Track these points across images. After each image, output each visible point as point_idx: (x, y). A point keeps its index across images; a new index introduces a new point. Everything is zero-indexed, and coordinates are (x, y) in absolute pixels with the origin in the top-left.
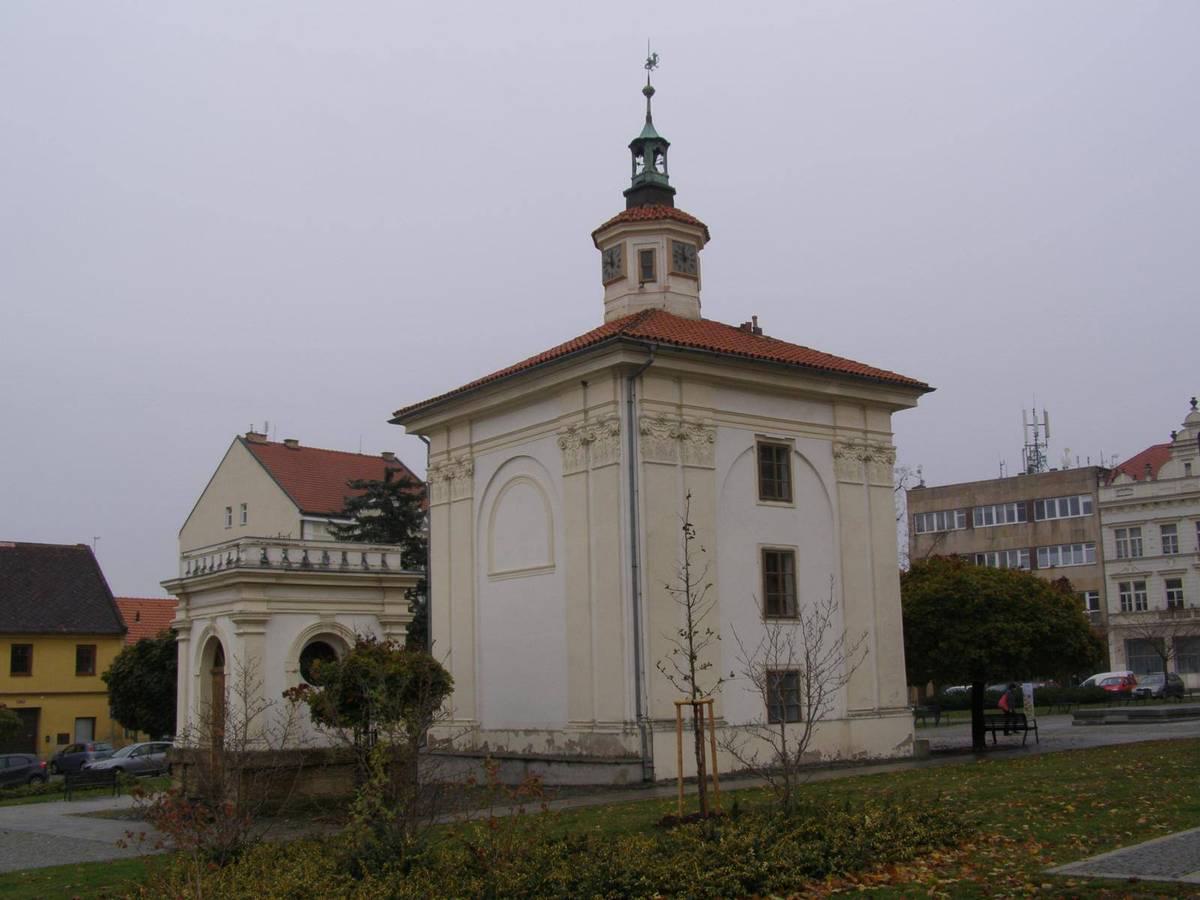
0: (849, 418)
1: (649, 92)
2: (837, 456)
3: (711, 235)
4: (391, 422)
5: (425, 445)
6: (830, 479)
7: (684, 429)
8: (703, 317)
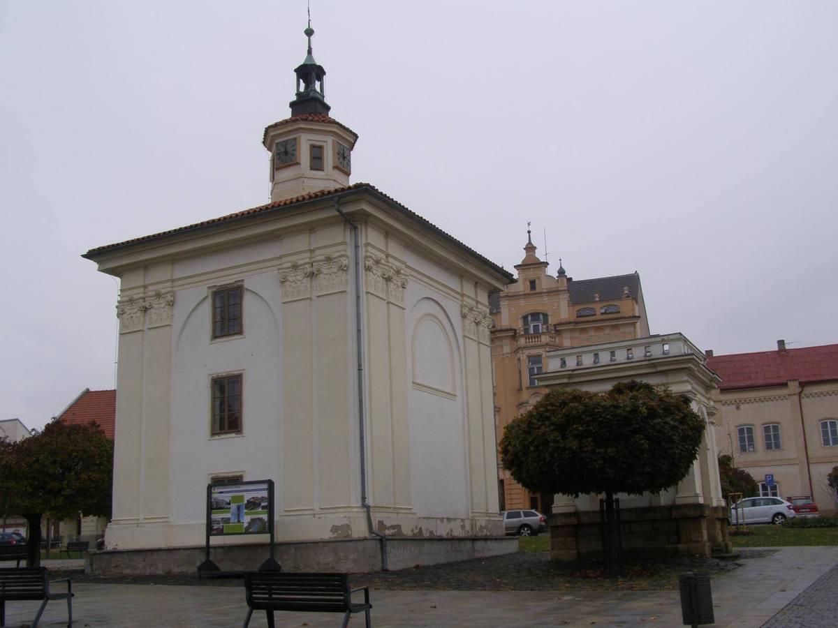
1: (309, 33)
7: (314, 270)
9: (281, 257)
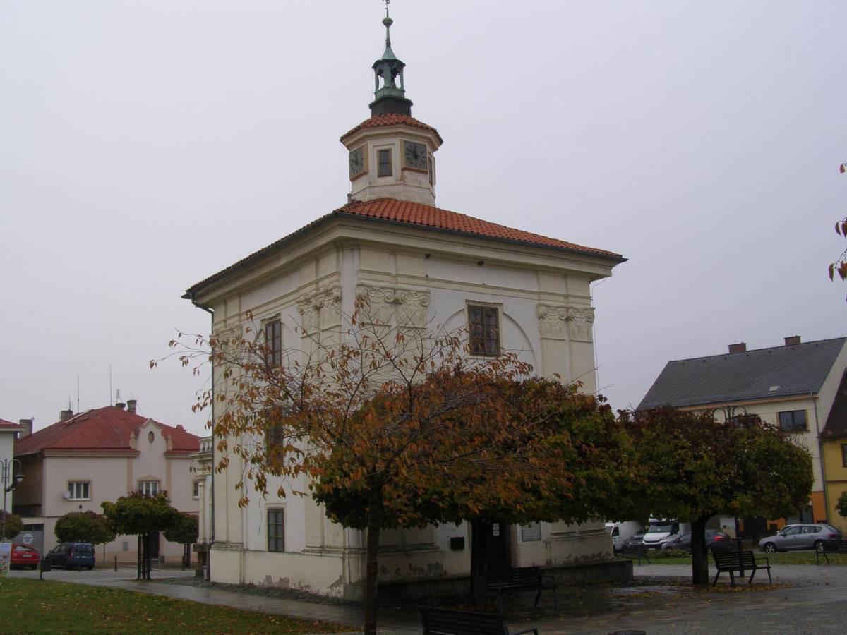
0: (554, 285)
1: (388, 23)
2: (541, 317)
3: (441, 136)
4: (183, 297)
5: (210, 314)
6: (534, 337)
7: (399, 295)
8: (437, 206)
9: (539, 293)
